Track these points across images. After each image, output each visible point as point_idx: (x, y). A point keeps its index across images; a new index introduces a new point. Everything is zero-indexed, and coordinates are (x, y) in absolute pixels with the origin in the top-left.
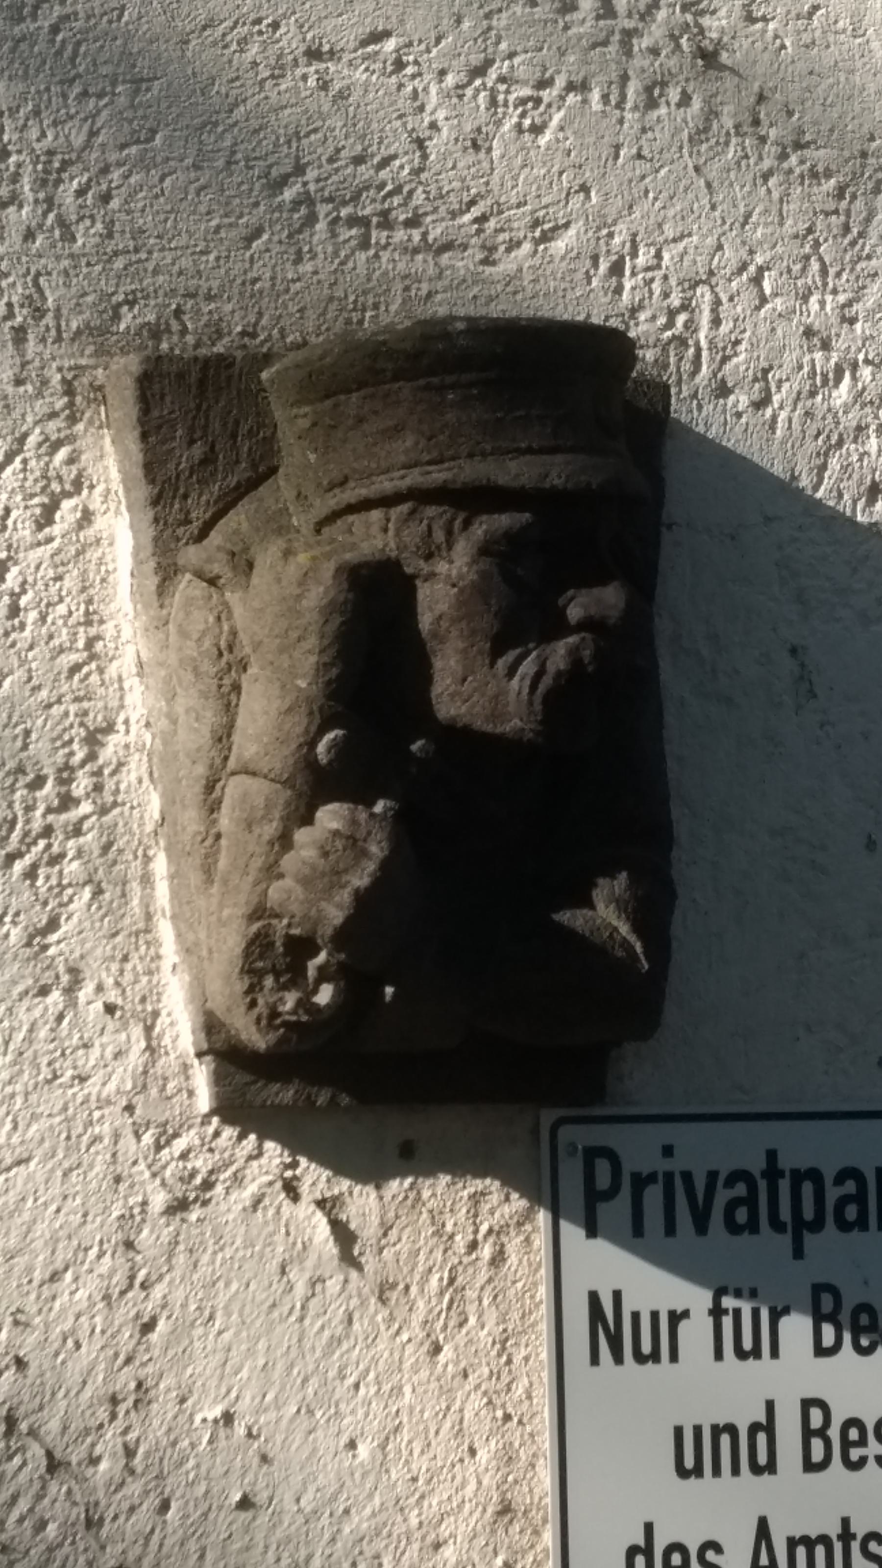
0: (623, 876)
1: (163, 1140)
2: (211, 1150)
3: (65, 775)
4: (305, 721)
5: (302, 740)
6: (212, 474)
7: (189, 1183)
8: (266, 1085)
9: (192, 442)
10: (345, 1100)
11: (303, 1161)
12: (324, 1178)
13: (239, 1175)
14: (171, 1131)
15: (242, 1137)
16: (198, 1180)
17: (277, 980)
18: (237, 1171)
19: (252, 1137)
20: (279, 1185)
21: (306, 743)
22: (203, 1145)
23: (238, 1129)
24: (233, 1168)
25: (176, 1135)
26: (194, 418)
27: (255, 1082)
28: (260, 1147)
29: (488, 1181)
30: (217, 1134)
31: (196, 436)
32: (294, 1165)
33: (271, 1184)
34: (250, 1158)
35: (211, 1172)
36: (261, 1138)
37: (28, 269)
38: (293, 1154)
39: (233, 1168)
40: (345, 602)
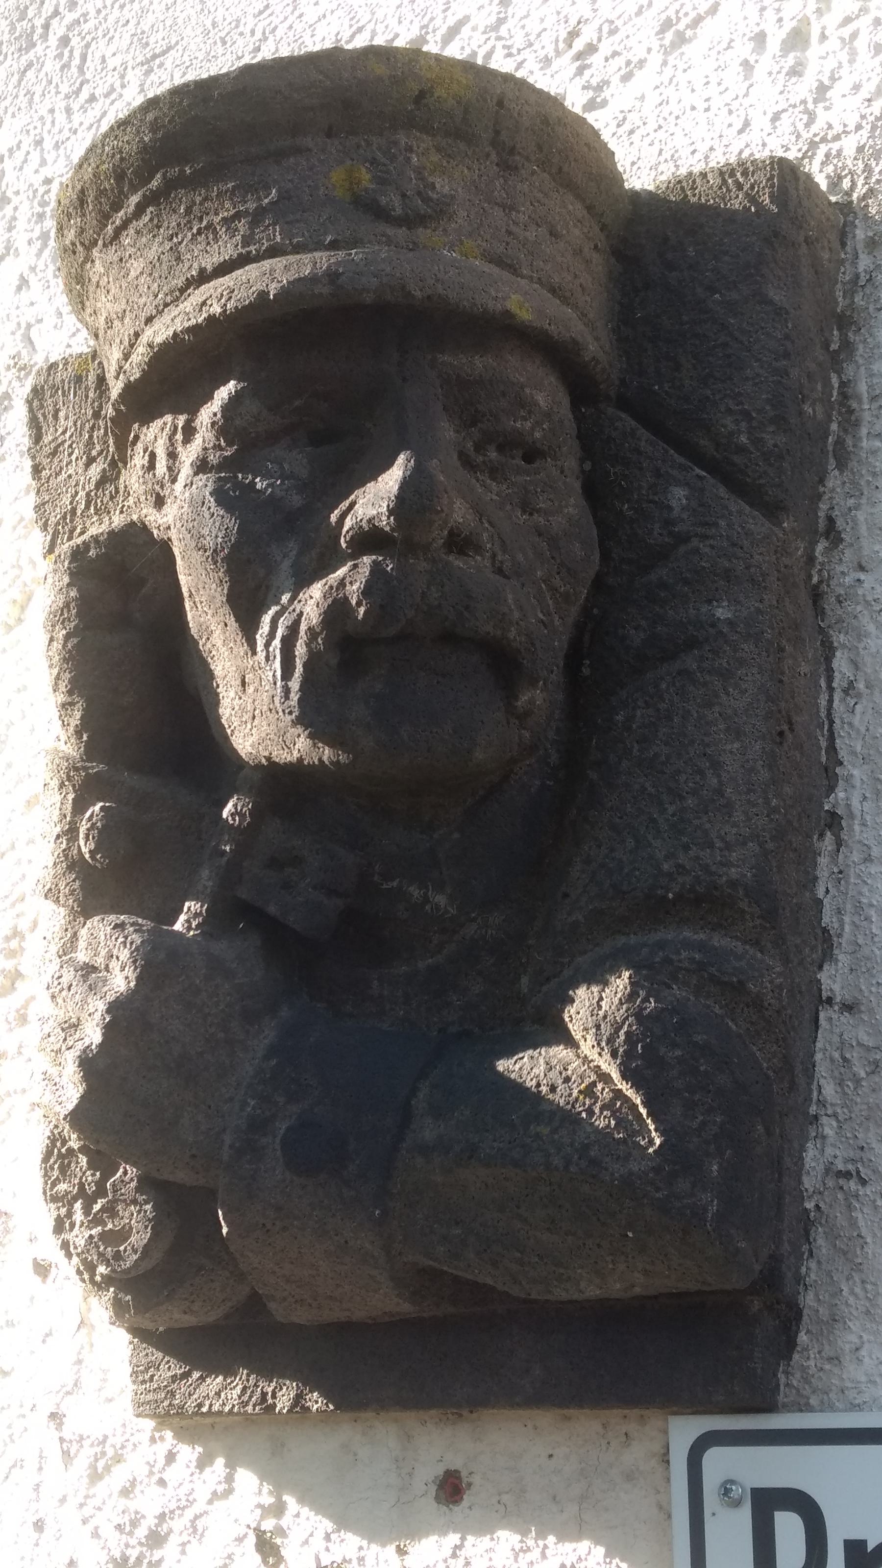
0: (621, 983)
1: (101, 1465)
2: (162, 1483)
3: (14, 944)
4: (58, 798)
5: (58, 829)
6: (112, 498)
7: (131, 1534)
8: (202, 1379)
9: (91, 461)
10: (316, 1402)
11: (290, 1500)
12: (320, 1535)
13: (200, 1524)
14: (110, 1452)
15: (203, 1463)
16: (141, 1532)
17: (87, 1210)
18: (196, 1517)
19: (220, 1462)
20: (252, 1539)
21: (65, 833)
22: (151, 1473)
23: (199, 1449)
24: (189, 1514)
25: (118, 1459)
26: (92, 429)
27: (186, 1375)
28: (229, 1479)
29: (584, 1545)
30: (171, 1457)
31: (94, 453)
32: (279, 1509)
33: (240, 1540)
34: (215, 1496)
35: (162, 1517)
36: (231, 1465)
37: (19, 324)
38: (278, 1490)
39: (189, 1514)
40: (67, 605)
